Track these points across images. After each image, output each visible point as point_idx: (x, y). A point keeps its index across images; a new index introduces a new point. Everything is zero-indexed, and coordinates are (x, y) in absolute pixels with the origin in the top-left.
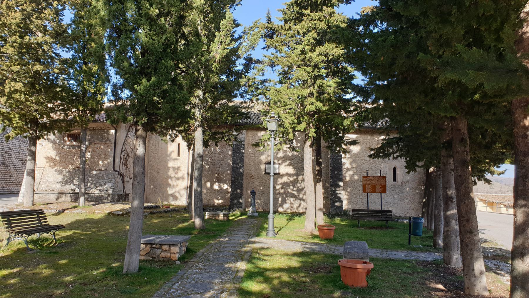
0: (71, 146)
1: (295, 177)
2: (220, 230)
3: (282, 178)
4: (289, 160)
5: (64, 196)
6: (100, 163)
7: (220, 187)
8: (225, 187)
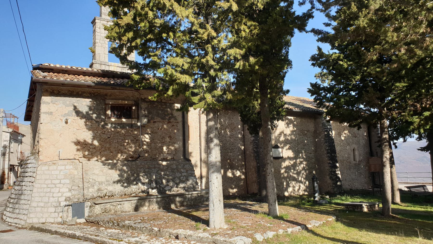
0: (119, 124)
1: (294, 161)
2: (134, 229)
3: (284, 162)
4: (289, 144)
5: (147, 204)
6: (165, 148)
7: (233, 174)
8: (238, 173)
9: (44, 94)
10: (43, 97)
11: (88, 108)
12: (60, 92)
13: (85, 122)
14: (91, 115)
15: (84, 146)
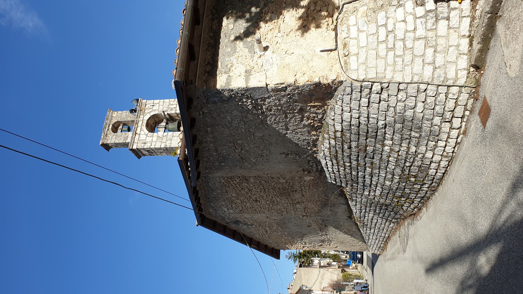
9: (212, 85)
10: (218, 87)
11: (239, 20)
12: (209, 63)
13: (266, 22)
14: (253, 14)
15: (310, 19)
